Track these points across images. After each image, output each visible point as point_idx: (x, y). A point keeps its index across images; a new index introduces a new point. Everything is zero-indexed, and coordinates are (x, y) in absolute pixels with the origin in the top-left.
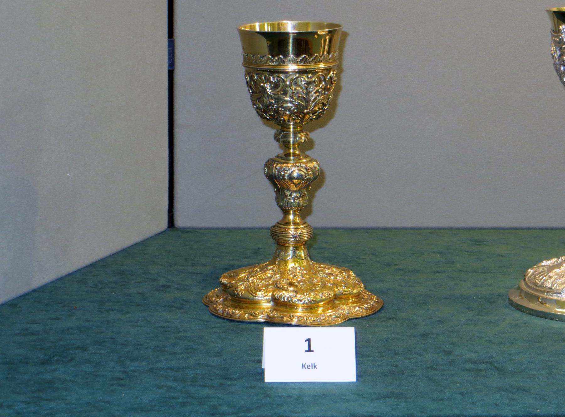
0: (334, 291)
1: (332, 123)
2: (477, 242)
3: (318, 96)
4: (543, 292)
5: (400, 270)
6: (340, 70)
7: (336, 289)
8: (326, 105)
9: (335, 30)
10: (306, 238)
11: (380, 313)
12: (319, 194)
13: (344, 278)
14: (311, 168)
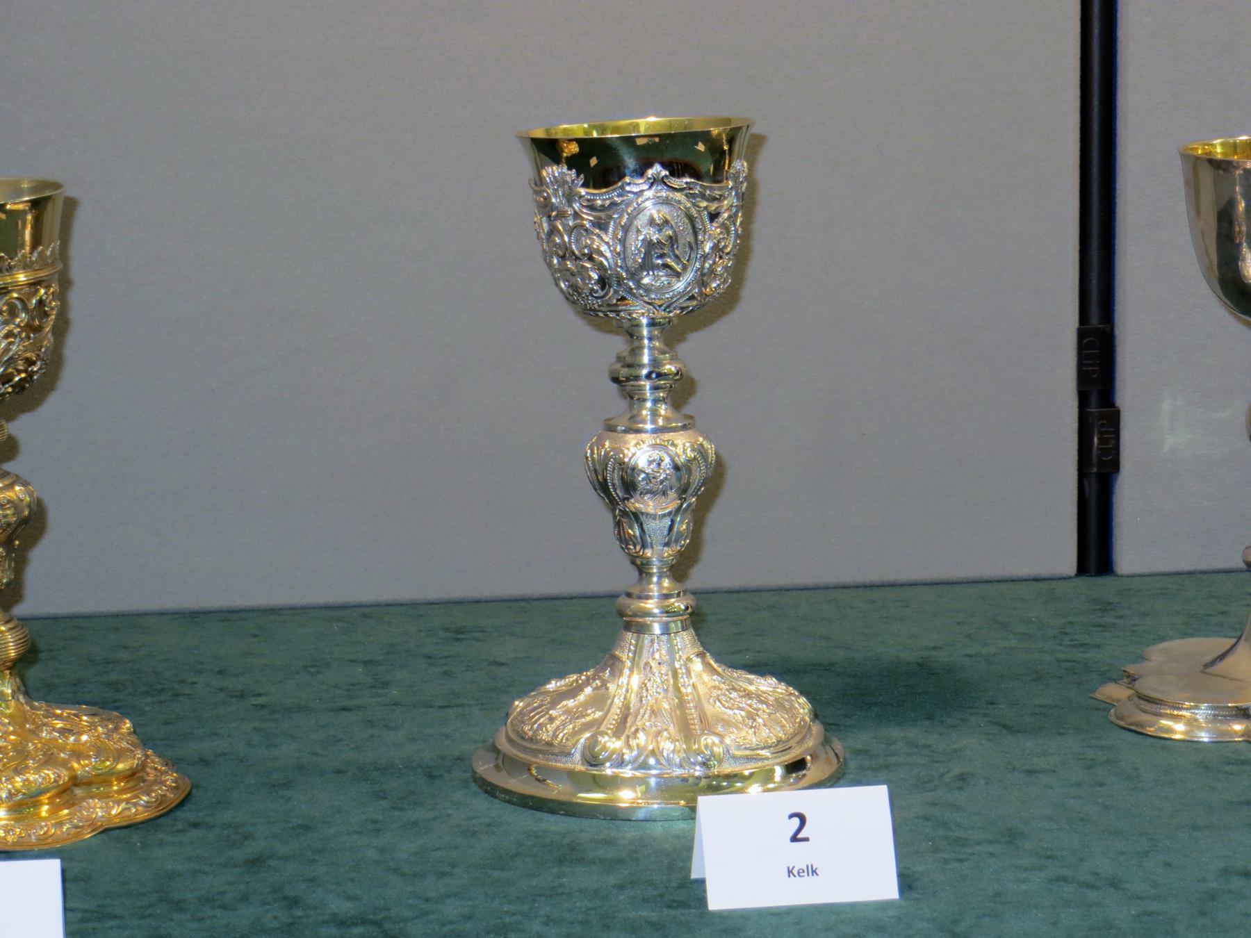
0: (72, 769)
1: (53, 401)
2: (459, 634)
3: (11, 343)
4: (535, 752)
5: (263, 706)
6: (65, 283)
7: (76, 765)
8: (34, 363)
9: (49, 198)
10: (13, 654)
11: (179, 813)
12: (39, 557)
13: (98, 737)
14: (9, 501)
